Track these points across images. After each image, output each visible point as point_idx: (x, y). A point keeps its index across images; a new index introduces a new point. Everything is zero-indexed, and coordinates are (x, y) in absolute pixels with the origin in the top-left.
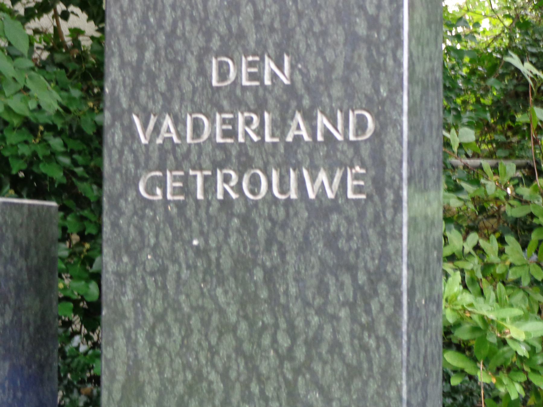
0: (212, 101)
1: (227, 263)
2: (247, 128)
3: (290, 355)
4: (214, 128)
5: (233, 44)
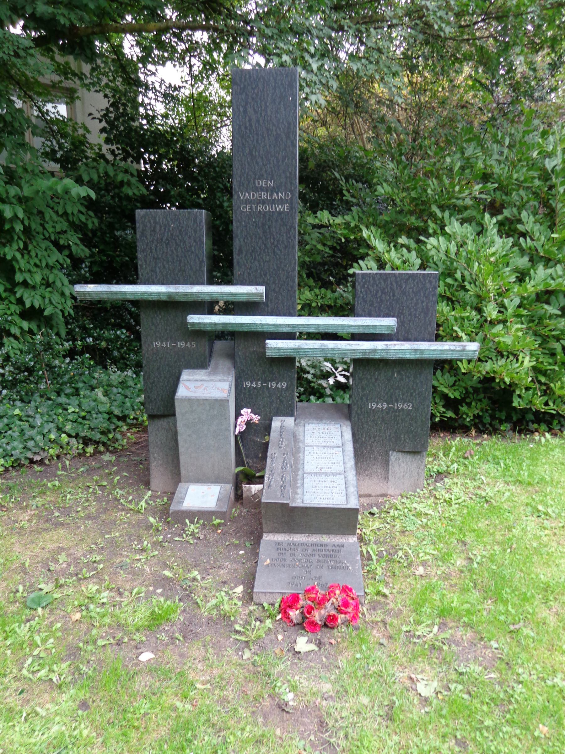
0: (257, 189)
2: (265, 195)
4: (257, 196)
5: (261, 177)
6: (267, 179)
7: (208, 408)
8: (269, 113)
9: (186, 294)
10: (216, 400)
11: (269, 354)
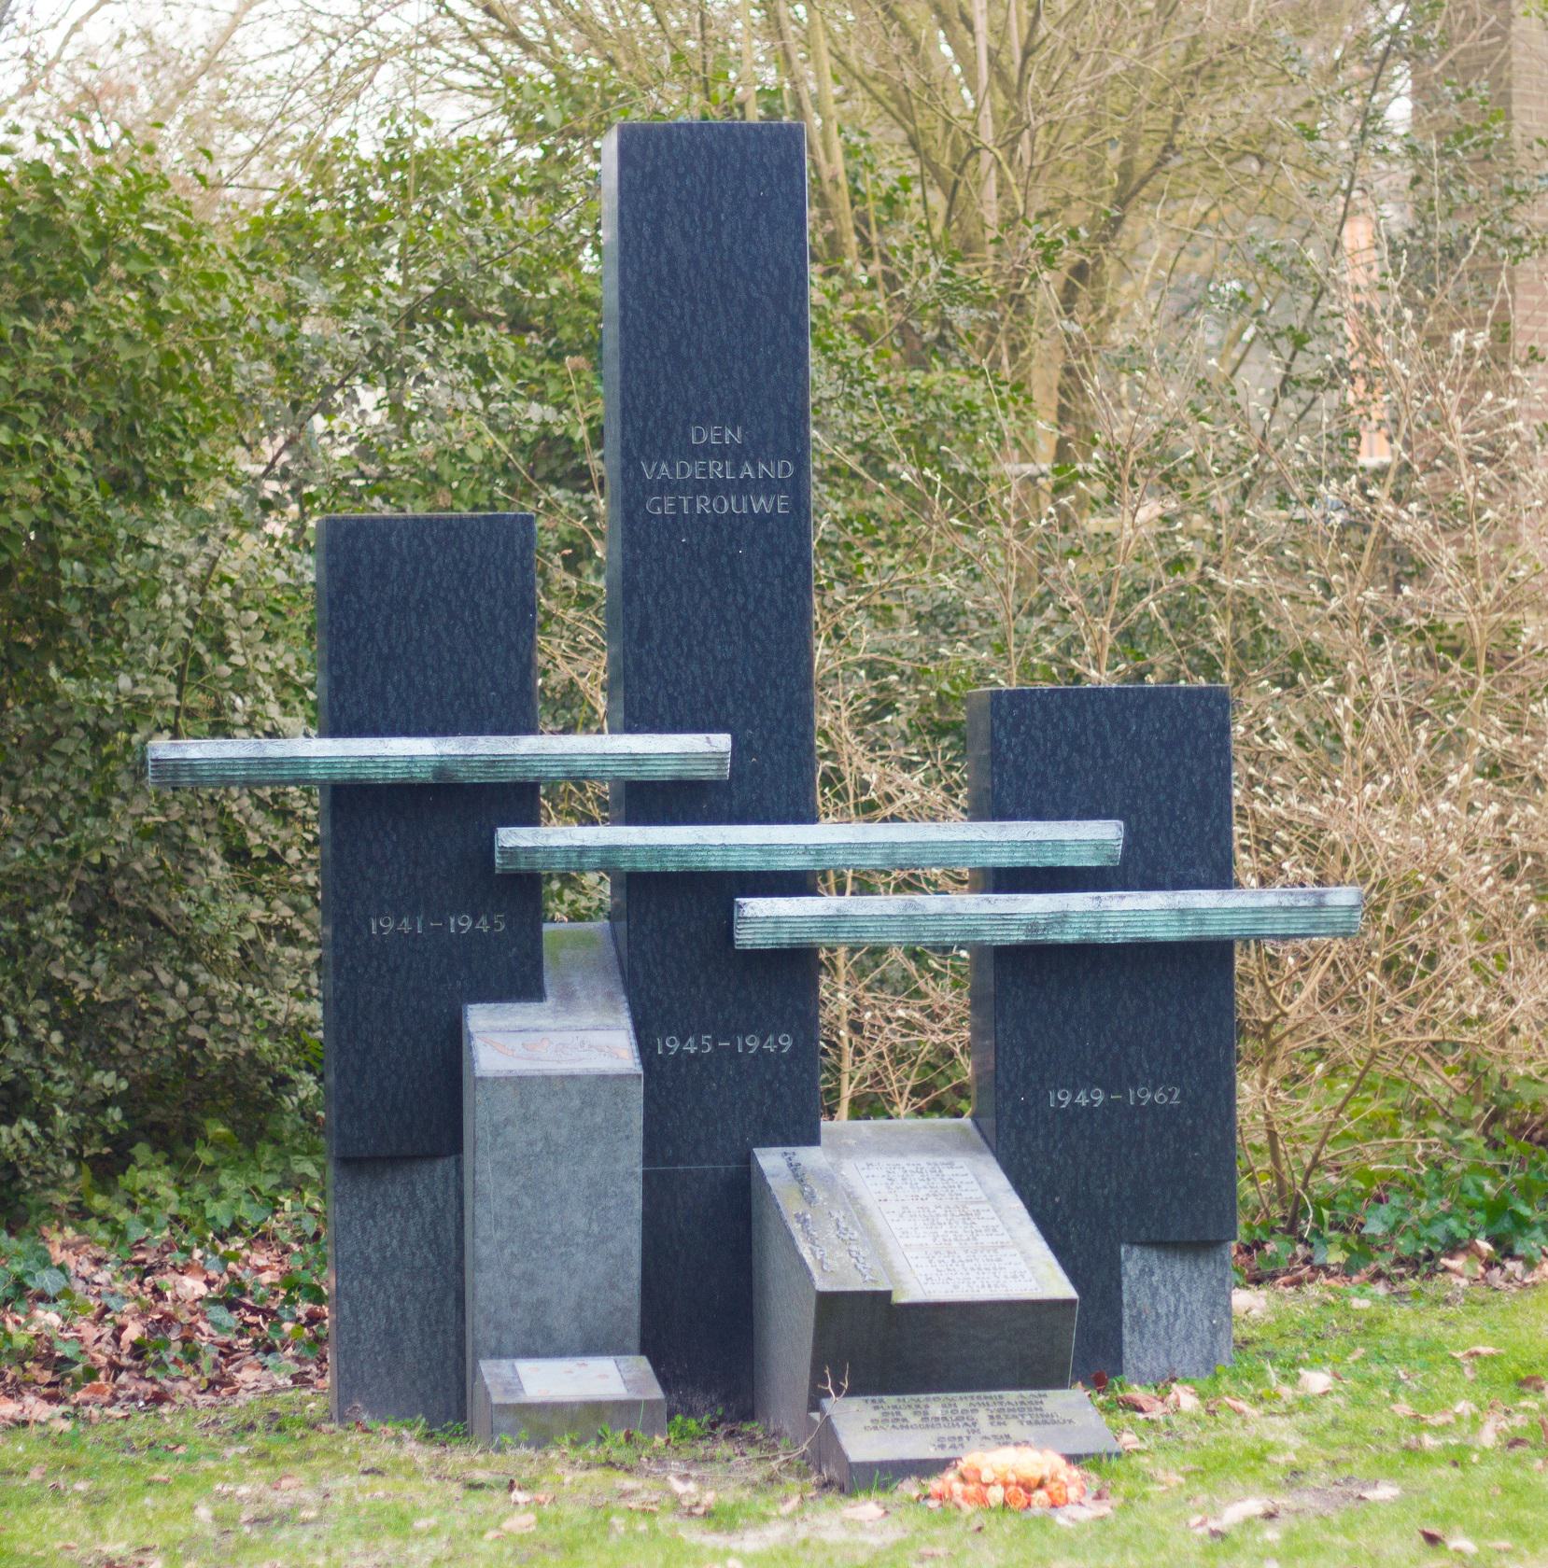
0: (694, 453)
1: (704, 552)
2: (717, 470)
3: (744, 608)
4: (694, 470)
5: (705, 418)
6: (723, 422)
7: (577, 1102)
8: (726, 240)
9: (493, 762)
10: (603, 1078)
11: (746, 937)
